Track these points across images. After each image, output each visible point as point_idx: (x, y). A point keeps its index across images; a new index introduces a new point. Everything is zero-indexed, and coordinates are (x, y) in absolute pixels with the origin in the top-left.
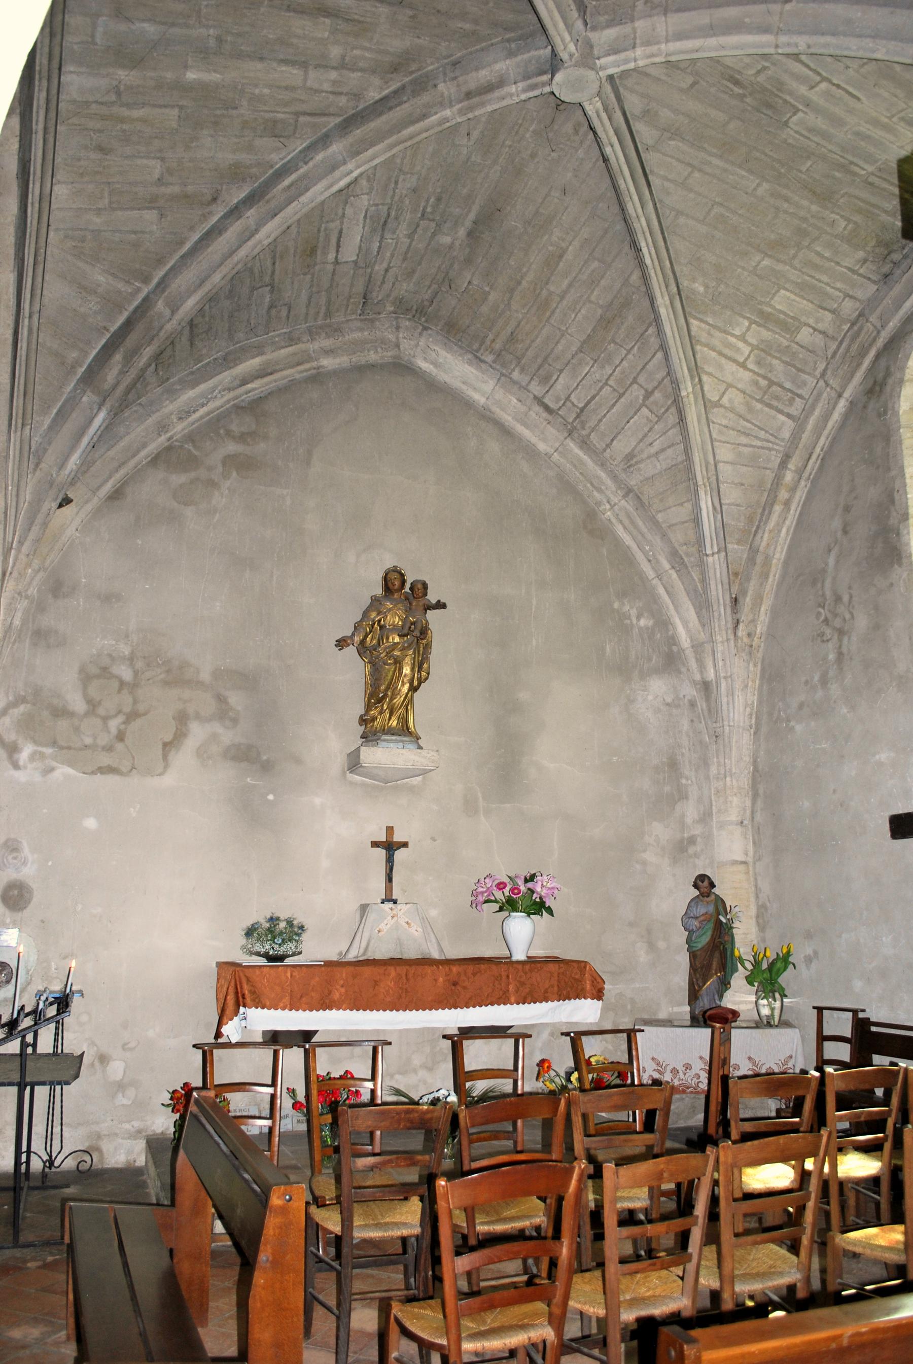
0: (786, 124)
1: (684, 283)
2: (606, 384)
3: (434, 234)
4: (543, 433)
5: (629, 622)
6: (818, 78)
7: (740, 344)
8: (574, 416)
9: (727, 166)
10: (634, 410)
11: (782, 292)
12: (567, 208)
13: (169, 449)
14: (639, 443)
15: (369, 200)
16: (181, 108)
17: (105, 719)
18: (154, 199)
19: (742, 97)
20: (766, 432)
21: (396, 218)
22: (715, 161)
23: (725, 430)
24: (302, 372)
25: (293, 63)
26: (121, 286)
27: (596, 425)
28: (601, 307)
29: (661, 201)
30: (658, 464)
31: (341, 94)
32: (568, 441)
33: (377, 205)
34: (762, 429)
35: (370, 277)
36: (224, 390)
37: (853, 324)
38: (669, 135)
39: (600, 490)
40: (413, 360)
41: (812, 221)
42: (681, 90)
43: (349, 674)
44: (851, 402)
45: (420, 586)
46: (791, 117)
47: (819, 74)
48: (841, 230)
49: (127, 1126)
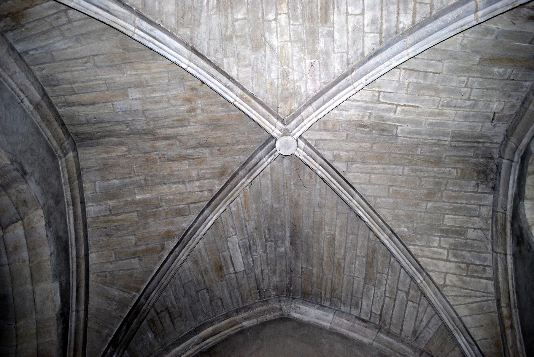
0: (397, 135)
1: (396, 230)
2: (385, 296)
3: (275, 248)
4: (364, 333)
6: (395, 107)
7: (440, 250)
8: (378, 320)
9: (384, 166)
10: (405, 305)
11: (447, 216)
12: (325, 214)
14: (415, 323)
15: (237, 238)
16: (137, 211)
18: (135, 253)
19: (370, 132)
20: (479, 291)
21: (254, 244)
22: (378, 166)
23: (456, 298)
25: (178, 183)
26: (126, 295)
27: (391, 321)
28: (364, 257)
29: (364, 195)
30: (430, 331)
31: (204, 191)
32: (379, 334)
33: (242, 240)
34: (476, 291)
35: (256, 278)
37: (492, 218)
38: (350, 163)
41: (439, 176)
42: (344, 141)
44: (513, 255)
46: (396, 131)
47: (394, 104)
48: (456, 174)
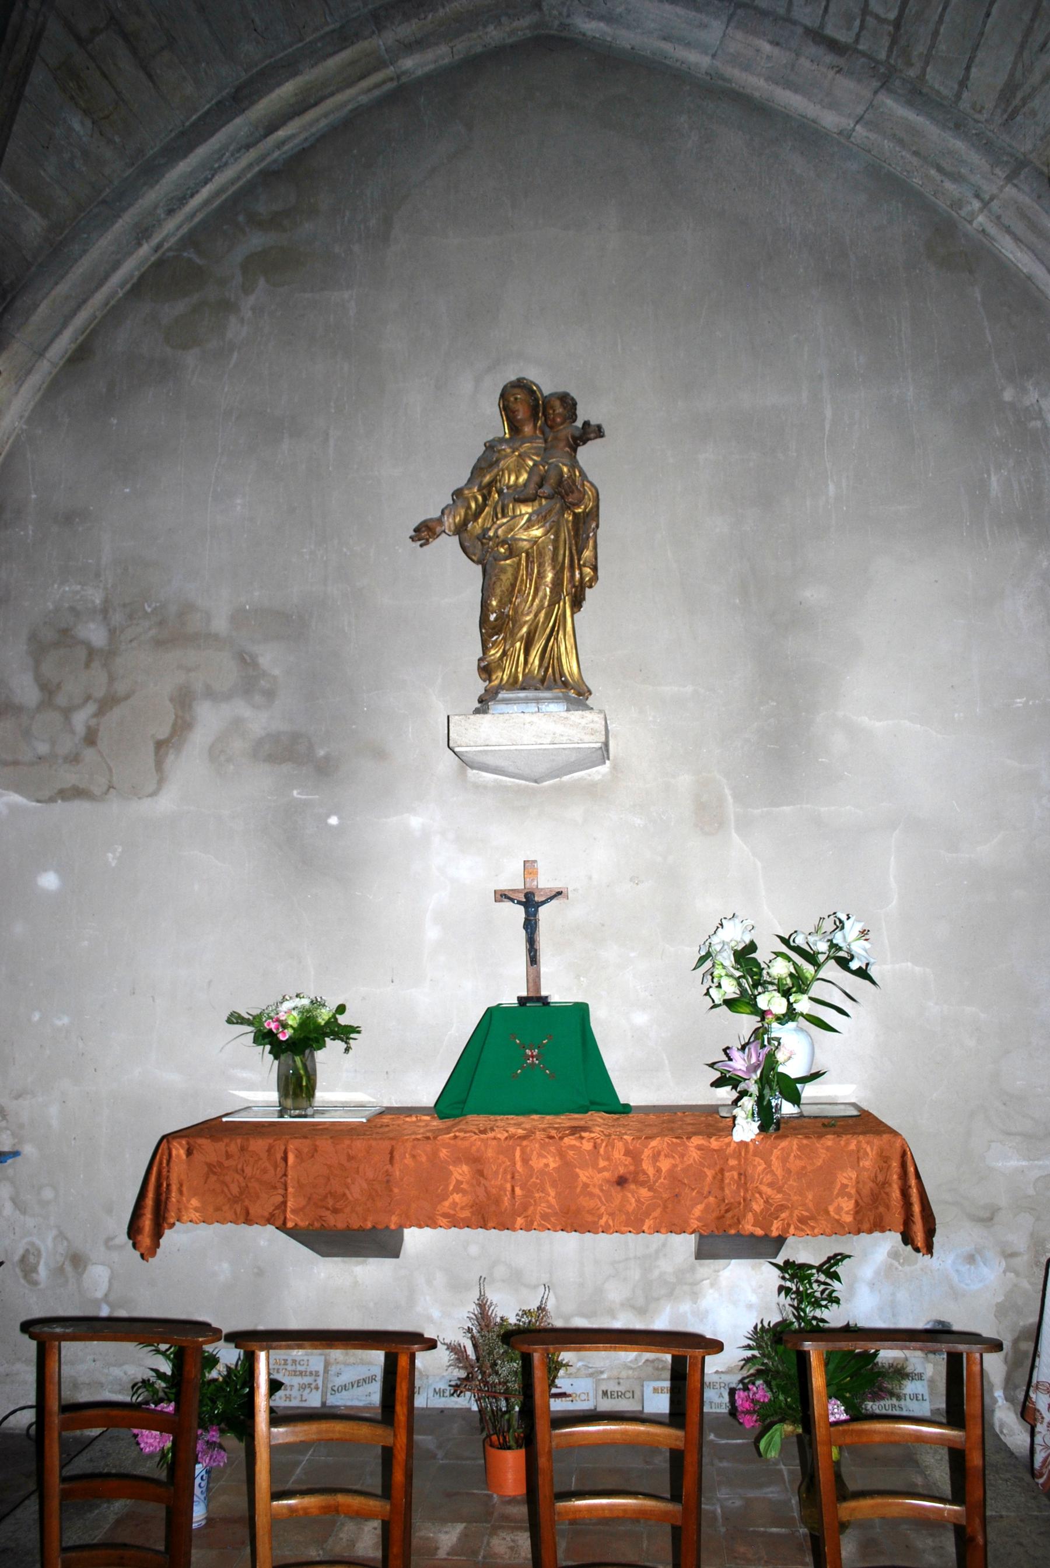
5: (1038, 424)
8: (886, 42)
13: (159, 264)
17: (67, 712)
24: (369, 90)
36: (239, 150)
39: (957, 178)
40: (568, 21)
43: (454, 583)
45: (557, 404)
49: (117, 1372)
